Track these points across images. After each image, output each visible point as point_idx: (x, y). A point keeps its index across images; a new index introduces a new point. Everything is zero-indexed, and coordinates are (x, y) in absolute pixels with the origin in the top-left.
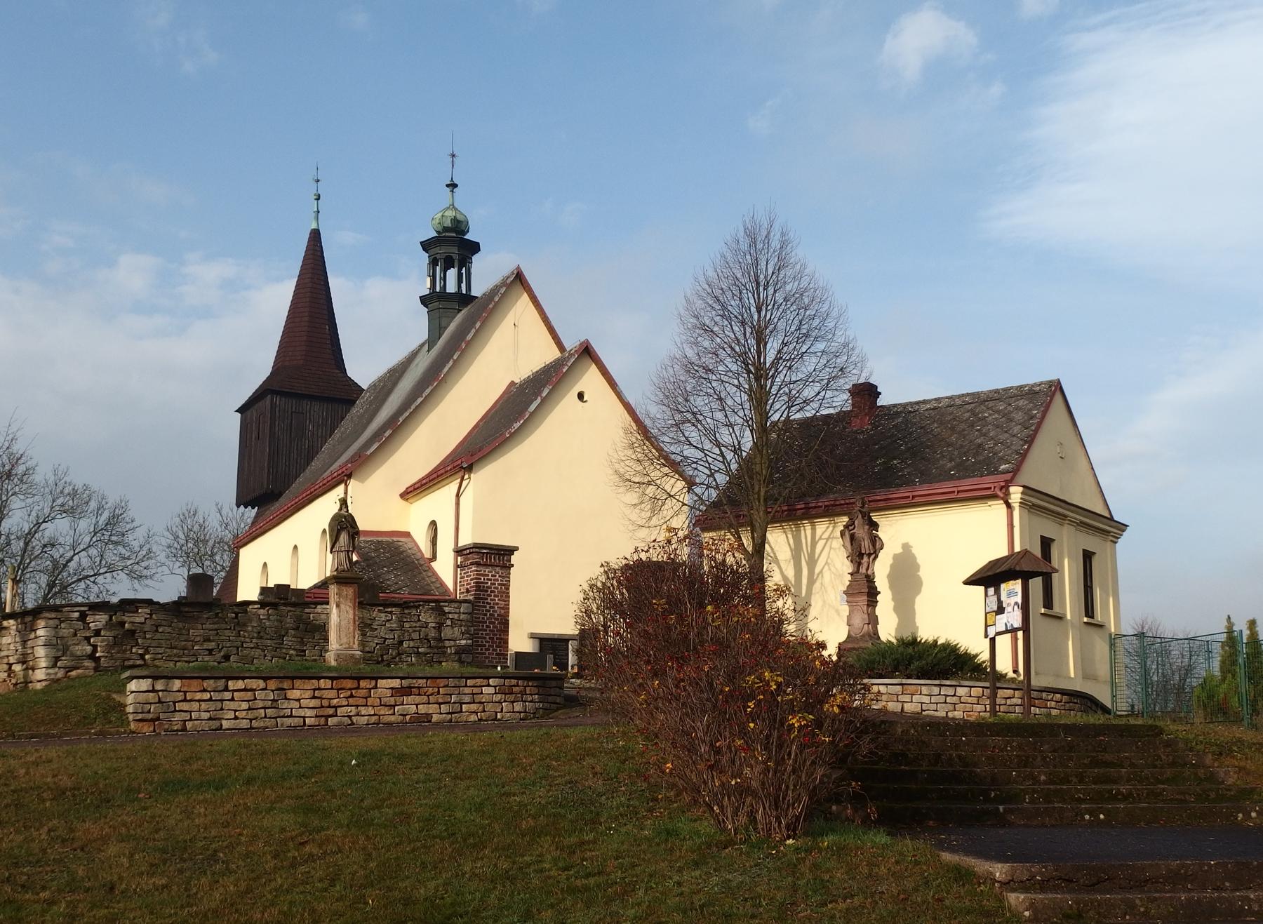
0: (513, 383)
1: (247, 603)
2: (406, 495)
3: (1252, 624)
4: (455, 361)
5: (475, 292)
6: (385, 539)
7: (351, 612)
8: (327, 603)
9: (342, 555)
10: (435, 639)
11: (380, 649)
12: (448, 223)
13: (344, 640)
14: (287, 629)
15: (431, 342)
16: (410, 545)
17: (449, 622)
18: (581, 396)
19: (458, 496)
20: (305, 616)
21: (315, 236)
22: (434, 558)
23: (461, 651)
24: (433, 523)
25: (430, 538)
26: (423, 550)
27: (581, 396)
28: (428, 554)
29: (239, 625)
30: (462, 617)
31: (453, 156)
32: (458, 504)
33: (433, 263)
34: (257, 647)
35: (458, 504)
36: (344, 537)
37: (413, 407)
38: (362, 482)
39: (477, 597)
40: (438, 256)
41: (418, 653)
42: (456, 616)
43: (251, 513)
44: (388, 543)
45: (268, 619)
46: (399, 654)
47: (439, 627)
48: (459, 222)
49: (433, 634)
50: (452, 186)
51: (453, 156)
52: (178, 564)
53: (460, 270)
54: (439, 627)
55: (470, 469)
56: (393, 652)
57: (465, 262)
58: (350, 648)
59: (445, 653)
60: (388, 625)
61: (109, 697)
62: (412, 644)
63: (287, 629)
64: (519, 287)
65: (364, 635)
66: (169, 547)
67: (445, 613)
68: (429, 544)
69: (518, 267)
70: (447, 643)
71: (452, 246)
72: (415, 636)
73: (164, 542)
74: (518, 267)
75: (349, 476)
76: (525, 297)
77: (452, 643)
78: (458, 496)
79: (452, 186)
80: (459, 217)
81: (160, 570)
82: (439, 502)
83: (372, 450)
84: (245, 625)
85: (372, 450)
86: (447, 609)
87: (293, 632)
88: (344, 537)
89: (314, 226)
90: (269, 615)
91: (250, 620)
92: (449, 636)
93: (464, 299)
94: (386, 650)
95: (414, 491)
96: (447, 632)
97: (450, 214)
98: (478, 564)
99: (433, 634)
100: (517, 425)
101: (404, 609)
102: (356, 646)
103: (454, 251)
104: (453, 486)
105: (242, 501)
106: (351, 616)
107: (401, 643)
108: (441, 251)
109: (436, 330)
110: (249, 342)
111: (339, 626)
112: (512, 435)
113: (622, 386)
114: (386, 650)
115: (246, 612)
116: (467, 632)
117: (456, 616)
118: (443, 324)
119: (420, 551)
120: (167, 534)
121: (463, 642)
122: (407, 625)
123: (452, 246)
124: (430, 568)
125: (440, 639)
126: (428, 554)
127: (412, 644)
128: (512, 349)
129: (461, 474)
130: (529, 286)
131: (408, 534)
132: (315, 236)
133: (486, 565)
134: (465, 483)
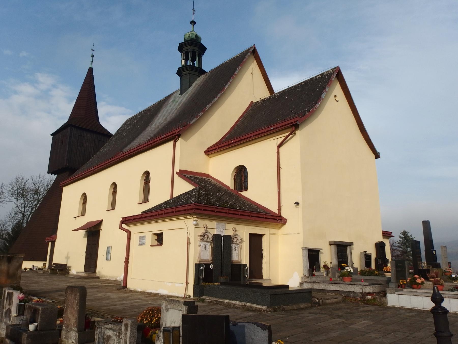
3: (426, 225)
21: (91, 71)
31: (194, 10)
37: (213, 102)
43: (54, 177)
50: (193, 23)
51: (194, 10)
52: (13, 198)
61: (40, 299)
66: (10, 191)
69: (254, 46)
73: (8, 189)
74: (254, 46)
75: (179, 136)
81: (6, 199)
89: (91, 66)
95: (212, 151)
105: (50, 171)
110: (62, 109)
120: (9, 186)
132: (91, 71)
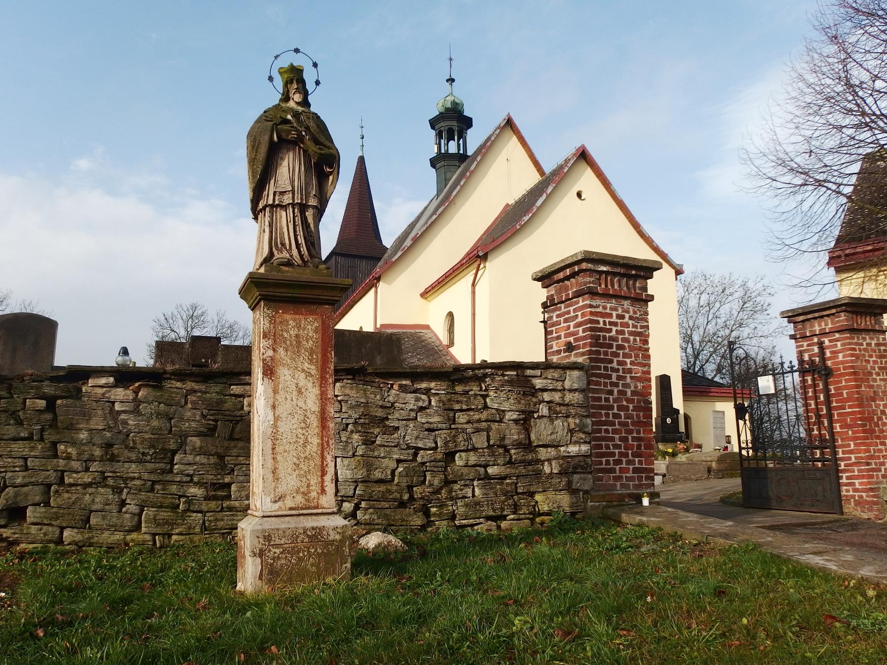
0: (507, 205)
1: (79, 375)
2: (425, 294)
4: (462, 187)
5: (469, 154)
6: (408, 331)
7: (313, 393)
8: (249, 373)
9: (284, 218)
10: (518, 445)
11: (407, 473)
12: (449, 105)
13: (290, 481)
14: (183, 437)
15: (438, 195)
16: (430, 335)
17: (544, 410)
18: (579, 195)
19: (474, 285)
20: (229, 404)
22: (451, 343)
23: (572, 467)
24: (451, 315)
25: (447, 328)
26: (442, 339)
27: (579, 195)
28: (445, 342)
29: (54, 426)
30: (568, 397)
31: (451, 59)
32: (473, 293)
33: (439, 135)
34: (102, 481)
35: (473, 293)
36: (289, 171)
38: (390, 284)
39: (595, 358)
40: (442, 129)
41: (487, 477)
42: (557, 397)
44: (412, 334)
45: (136, 411)
46: (447, 483)
47: (526, 420)
48: (457, 104)
49: (514, 434)
50: (451, 80)
51: (451, 59)
53: (458, 141)
54: (526, 420)
55: (485, 258)
56: (434, 480)
57: (462, 135)
58: (309, 509)
59: (538, 474)
60: (421, 419)
62: (473, 458)
63: (183, 437)
64: (509, 132)
65: (369, 442)
67: (534, 392)
68: (446, 333)
70: (543, 453)
71: (452, 122)
72: (479, 441)
76: (515, 139)
77: (552, 452)
78: (474, 285)
79: (451, 80)
80: (457, 101)
82: (456, 295)
83: (396, 257)
84: (71, 427)
85: (396, 257)
86: (538, 383)
87: (196, 441)
88: (289, 171)
89: (361, 154)
90: (137, 402)
91: (87, 415)
92: (547, 440)
93: (462, 158)
94: (419, 474)
96: (541, 431)
97: (450, 98)
98: (593, 293)
99: (514, 434)
100: (526, 218)
101: (454, 382)
102: (328, 501)
103: (454, 124)
104: (469, 278)
106: (312, 403)
107: (450, 456)
108: (443, 125)
109: (442, 183)
111: (274, 438)
112: (522, 227)
113: (615, 185)
114: (419, 474)
115: (77, 394)
116: (581, 428)
117: (557, 397)
118: (448, 176)
119: (438, 339)
121: (573, 449)
122: (462, 418)
123: (452, 122)
124: (448, 353)
125: (527, 446)
126: (445, 342)
127: (473, 458)
128: (503, 179)
129: (476, 265)
130: (517, 129)
131: (427, 327)
133: (606, 296)
134: (480, 273)
